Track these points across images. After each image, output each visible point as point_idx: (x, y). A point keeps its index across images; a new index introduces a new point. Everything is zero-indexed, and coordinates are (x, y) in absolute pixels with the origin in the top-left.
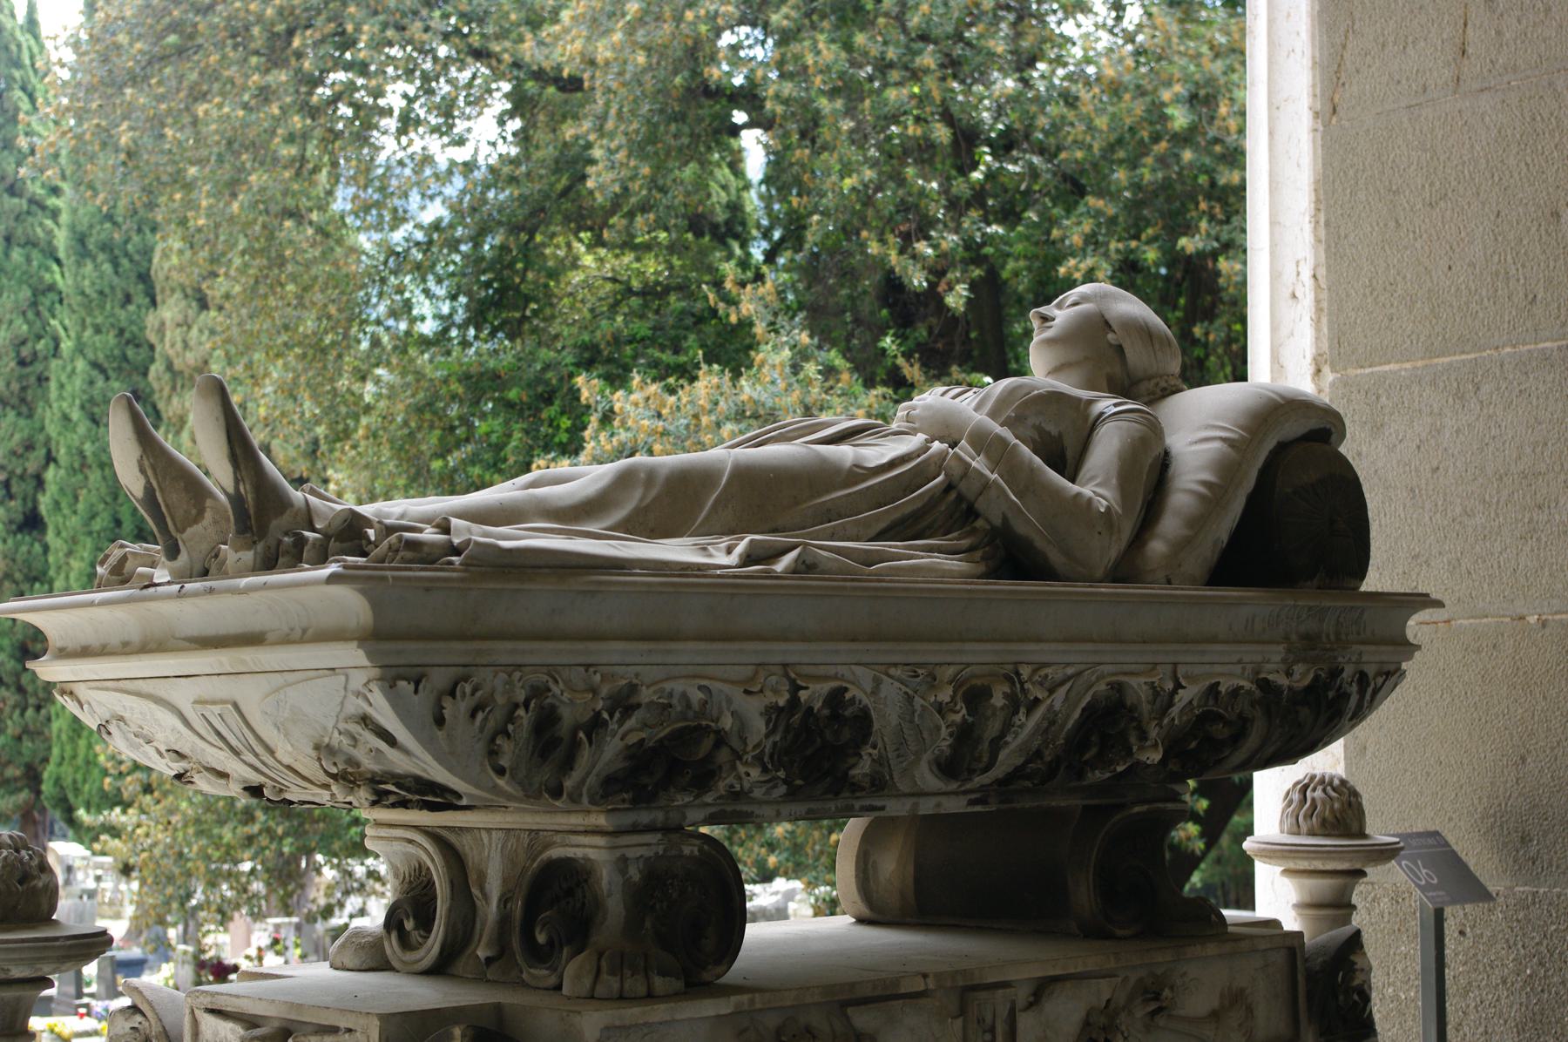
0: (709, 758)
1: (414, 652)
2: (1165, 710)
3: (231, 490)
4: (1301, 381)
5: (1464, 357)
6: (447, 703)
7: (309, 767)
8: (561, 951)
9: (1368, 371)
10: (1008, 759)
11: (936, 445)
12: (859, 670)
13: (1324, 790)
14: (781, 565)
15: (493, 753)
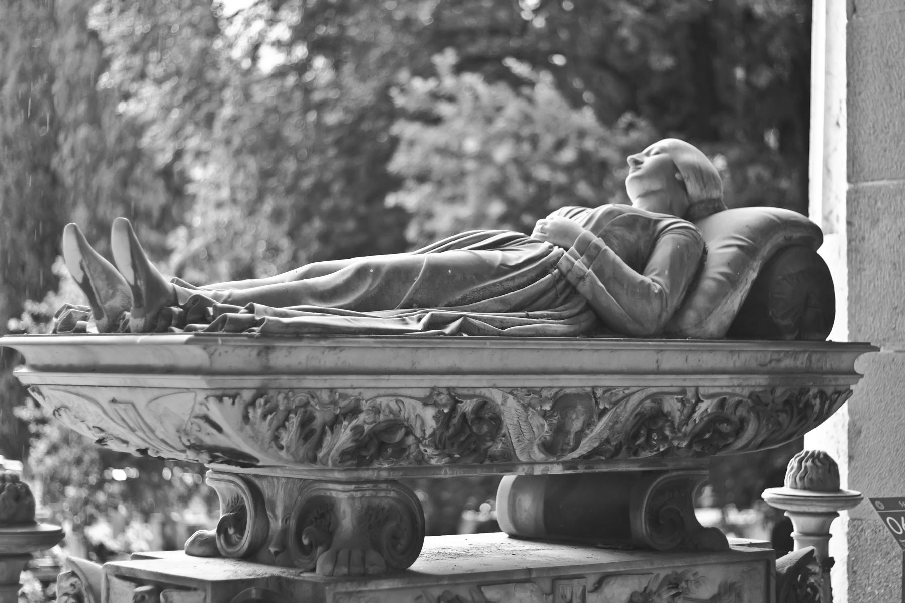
0: (402, 441)
1: (231, 382)
3: (132, 283)
6: (251, 410)
7: (173, 439)
10: (584, 448)
11: (556, 250)
12: (494, 391)
13: (813, 462)
14: (448, 330)
15: (276, 438)
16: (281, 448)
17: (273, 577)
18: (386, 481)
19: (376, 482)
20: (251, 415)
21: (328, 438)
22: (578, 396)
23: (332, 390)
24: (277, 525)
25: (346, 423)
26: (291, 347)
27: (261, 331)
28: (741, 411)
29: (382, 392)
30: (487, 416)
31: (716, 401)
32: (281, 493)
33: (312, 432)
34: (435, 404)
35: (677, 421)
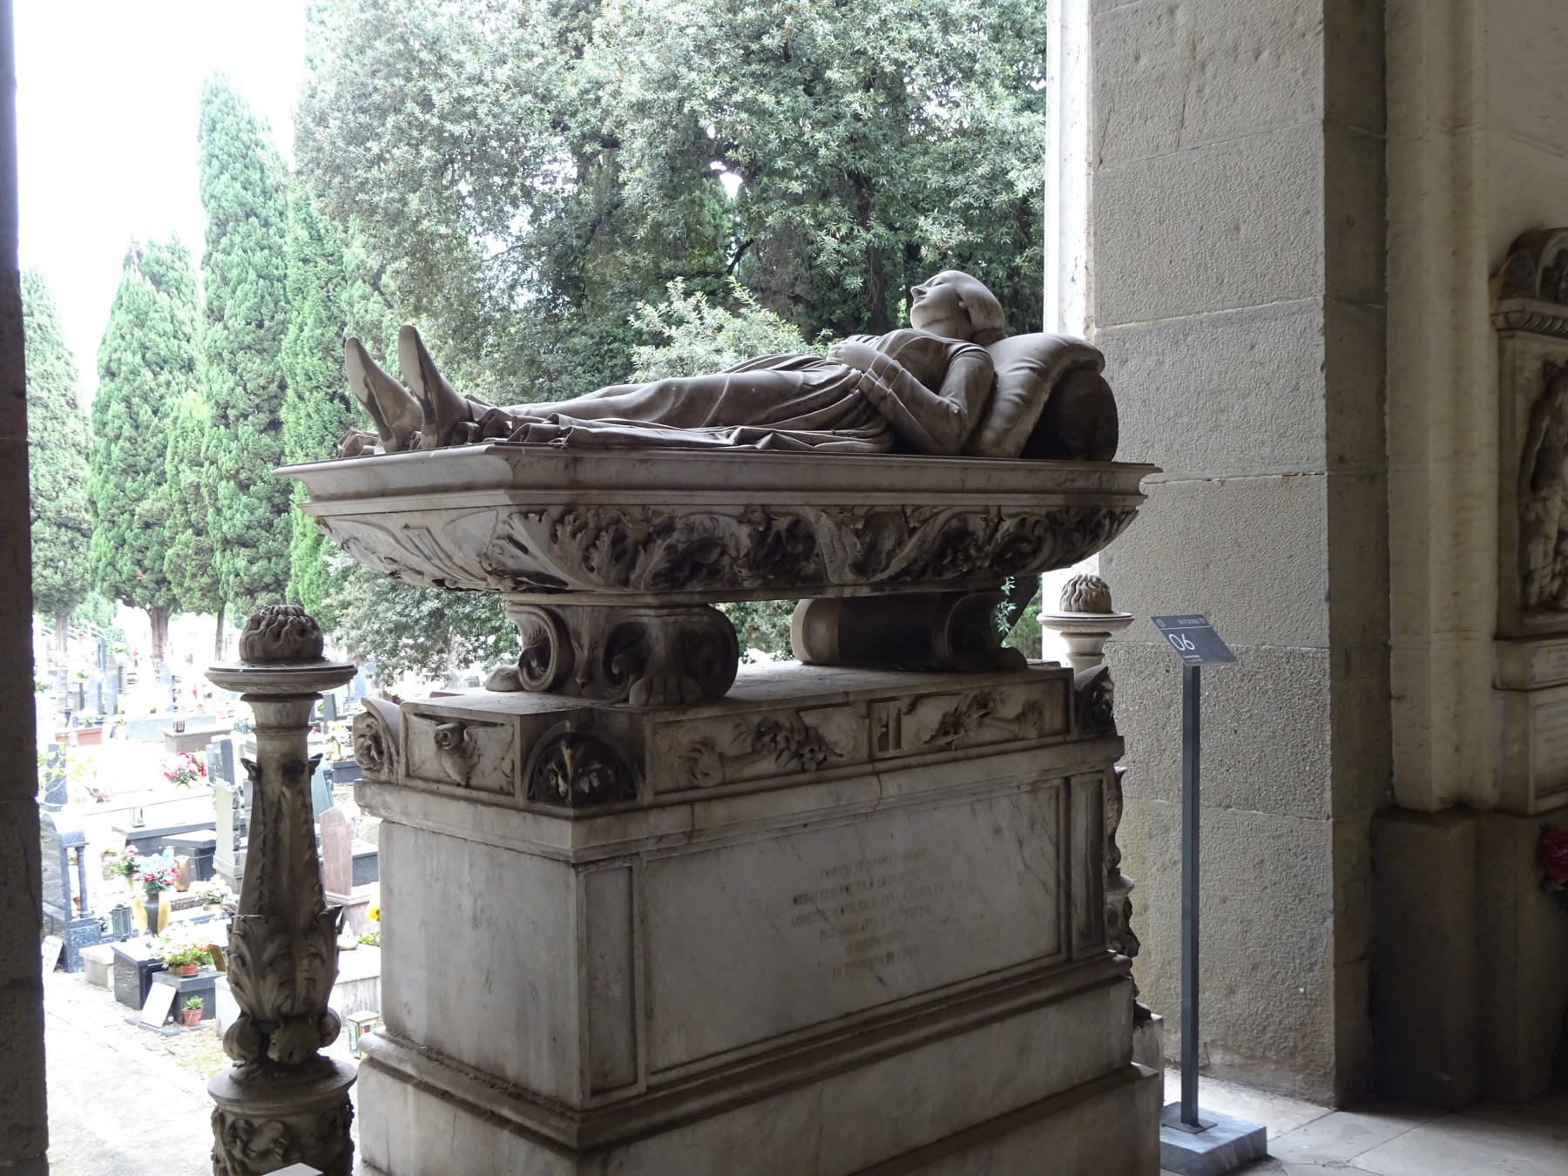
0: (717, 561)
1: (538, 497)
4: (1076, 331)
6: (559, 528)
10: (896, 566)
11: (854, 371)
14: (759, 446)
15: (586, 559)
16: (592, 570)
17: (584, 709)
19: (688, 606)
21: (642, 558)
22: (888, 514)
23: (644, 506)
24: (582, 655)
25: (659, 542)
28: (1039, 531)
29: (695, 509)
30: (799, 532)
32: (587, 623)
33: (624, 551)
34: (749, 522)
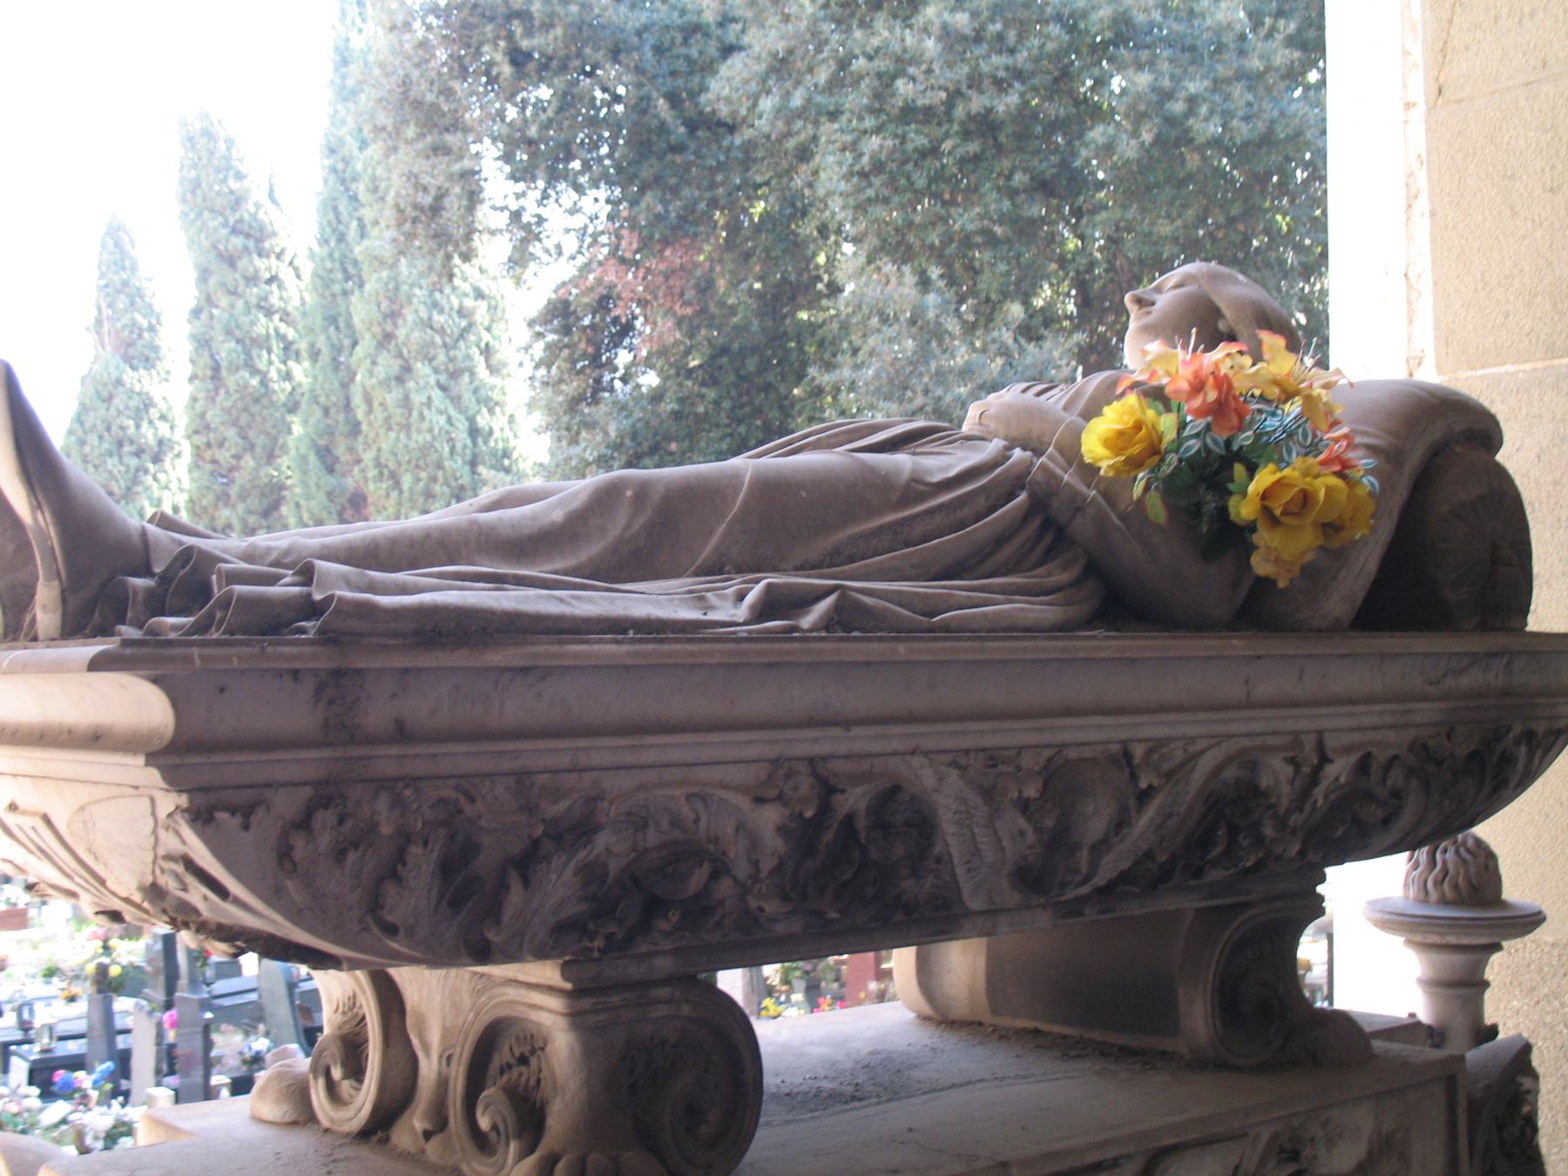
1: (247, 768)
2: (1306, 793)
5: (1470, 373)
8: (507, 1145)
9: (1480, 373)
10: (1109, 868)
11: (1017, 453)
12: (917, 761)
13: (1457, 852)
14: (807, 621)
15: (374, 905)
18: (668, 980)
19: (644, 985)
20: (298, 854)
23: (522, 778)
24: (429, 1069)
26: (406, 671)
27: (321, 631)
31: (1354, 758)
34: (780, 798)
35: (1285, 802)
